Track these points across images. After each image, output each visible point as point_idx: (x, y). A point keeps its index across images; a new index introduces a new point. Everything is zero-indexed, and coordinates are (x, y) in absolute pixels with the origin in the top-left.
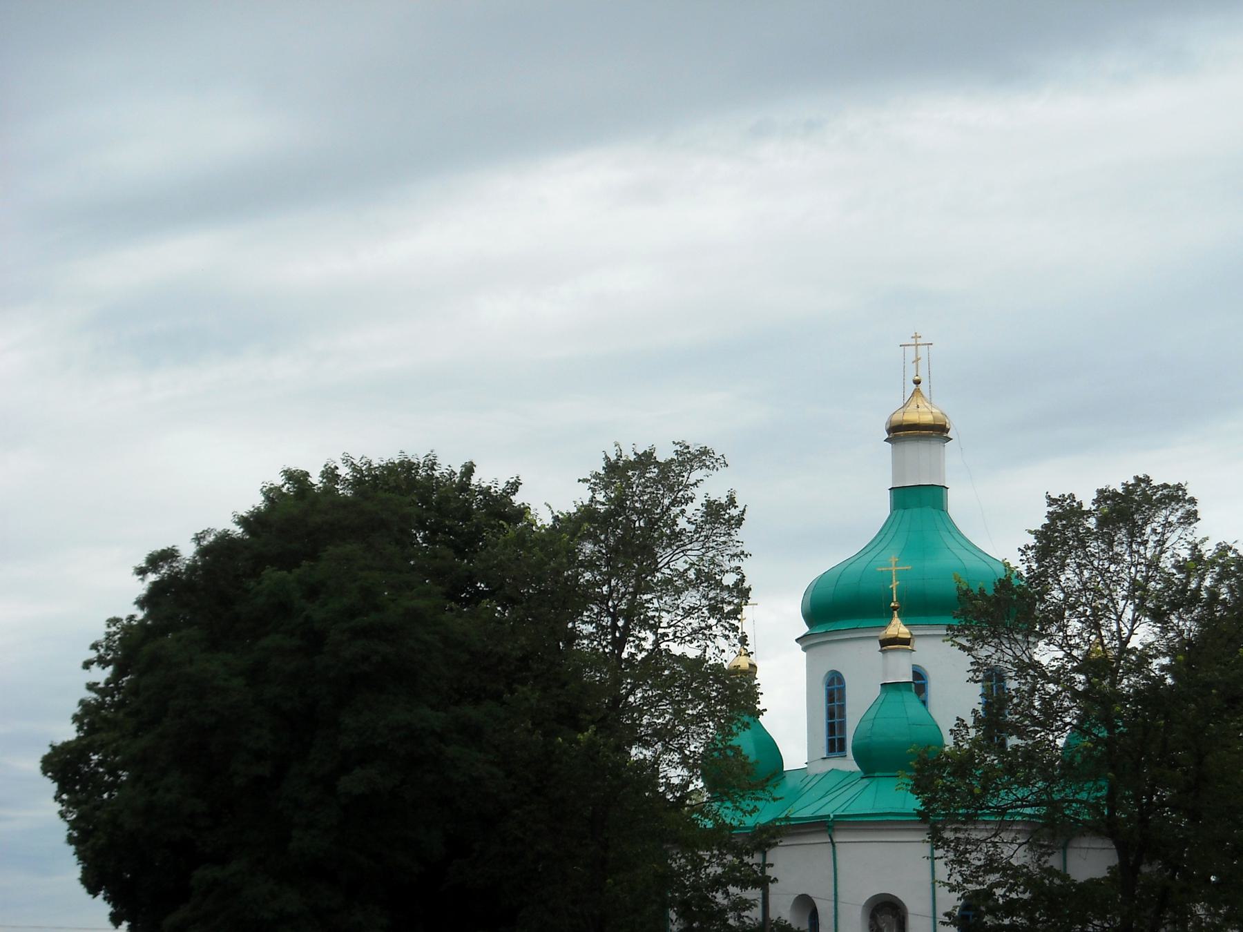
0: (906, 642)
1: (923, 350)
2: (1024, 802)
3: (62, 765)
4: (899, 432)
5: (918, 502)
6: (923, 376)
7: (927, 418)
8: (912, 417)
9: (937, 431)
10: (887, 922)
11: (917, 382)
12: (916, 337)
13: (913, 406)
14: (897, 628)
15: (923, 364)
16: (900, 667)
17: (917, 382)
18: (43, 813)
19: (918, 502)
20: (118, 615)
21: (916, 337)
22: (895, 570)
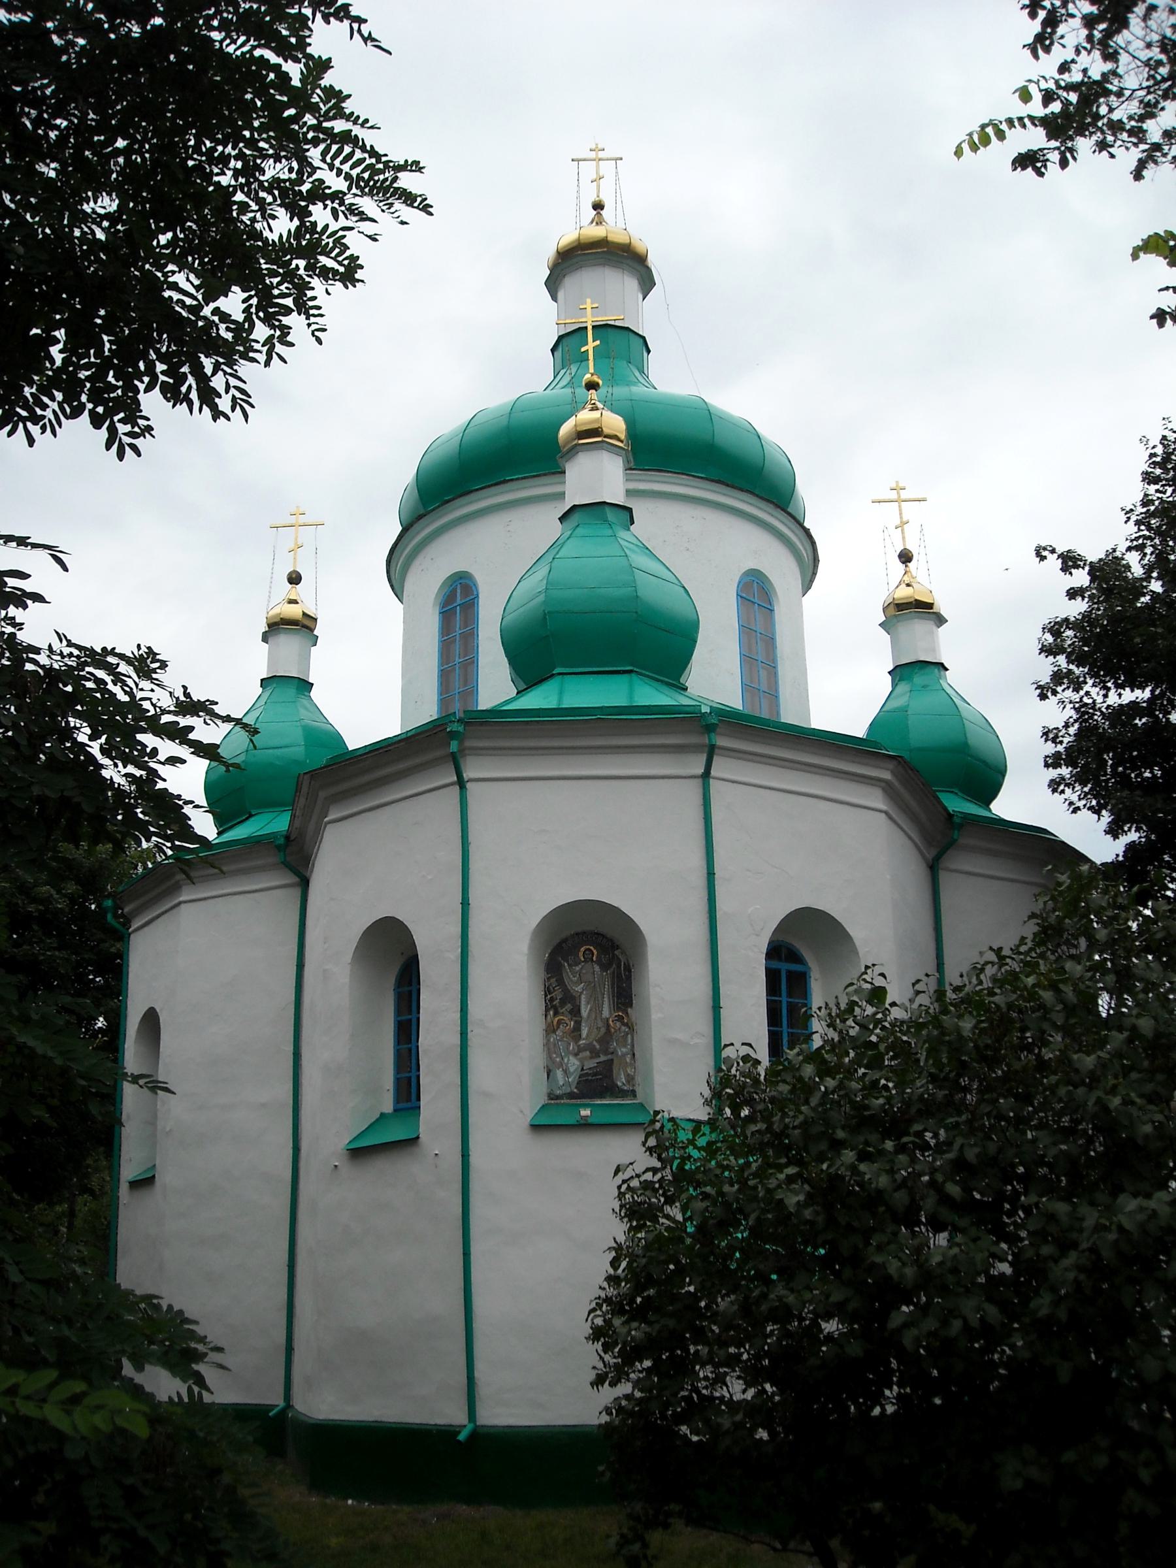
2: (597, 1009)
10: (585, 979)
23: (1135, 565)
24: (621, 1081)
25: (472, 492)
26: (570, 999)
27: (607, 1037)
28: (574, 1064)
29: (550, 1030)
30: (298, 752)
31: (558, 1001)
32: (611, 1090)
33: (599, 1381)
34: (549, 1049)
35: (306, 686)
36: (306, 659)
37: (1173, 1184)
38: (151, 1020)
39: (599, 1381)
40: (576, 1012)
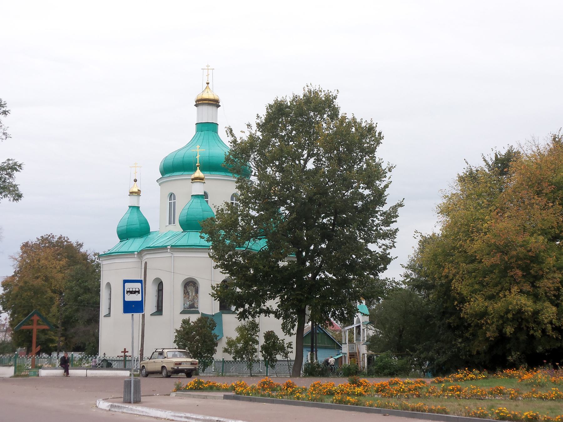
0: (202, 179)
1: (210, 71)
2: (192, 294)
3: (26, 247)
4: (200, 102)
5: (207, 128)
6: (210, 82)
7: (211, 97)
8: (206, 96)
9: (215, 103)
10: (191, 289)
11: (208, 84)
12: (208, 66)
13: (206, 91)
14: (198, 173)
15: (210, 77)
16: (198, 189)
17: (208, 84)
18: (17, 251)
19: (207, 128)
20: (54, 234)
21: (208, 66)
22: (200, 152)
23: (347, 120)
24: (196, 306)
25: (155, 417)
26: (188, 292)
27: (193, 299)
28: (188, 303)
29: (184, 297)
30: (138, 226)
31: (186, 293)
32: (194, 307)
33: (397, 230)
34: (184, 301)
35: (138, 207)
36: (138, 201)
37: (562, 174)
38: (109, 285)
39: (397, 230)
40: (189, 294)
